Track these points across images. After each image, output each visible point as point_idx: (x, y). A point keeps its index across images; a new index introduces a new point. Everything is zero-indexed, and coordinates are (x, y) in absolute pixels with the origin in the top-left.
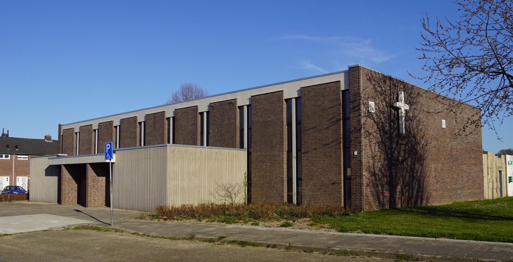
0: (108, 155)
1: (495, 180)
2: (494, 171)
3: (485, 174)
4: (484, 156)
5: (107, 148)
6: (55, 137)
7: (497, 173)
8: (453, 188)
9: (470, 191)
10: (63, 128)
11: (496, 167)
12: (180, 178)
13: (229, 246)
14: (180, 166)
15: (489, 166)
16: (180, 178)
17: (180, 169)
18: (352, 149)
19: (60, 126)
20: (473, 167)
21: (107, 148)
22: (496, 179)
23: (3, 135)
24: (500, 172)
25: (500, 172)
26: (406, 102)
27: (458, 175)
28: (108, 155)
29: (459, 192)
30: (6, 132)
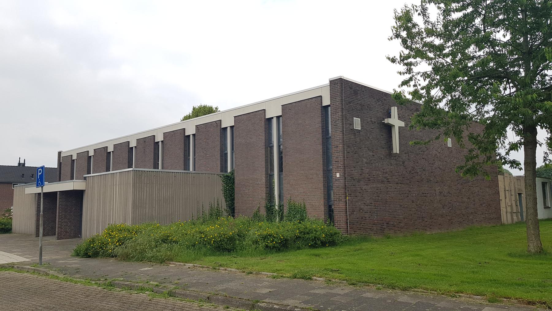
0: (39, 182)
1: (514, 203)
2: (513, 193)
3: (502, 196)
4: (500, 177)
5: (39, 174)
6: (54, 164)
7: (516, 196)
8: (464, 213)
9: (484, 216)
10: (62, 155)
11: (515, 190)
12: (147, 206)
13: (28, 275)
14: (148, 193)
15: (507, 189)
16: (147, 206)
17: (148, 195)
18: (334, 170)
19: (60, 153)
20: (487, 190)
21: (39, 174)
22: (516, 202)
23: (19, 164)
24: (520, 194)
25: (520, 194)
26: (400, 118)
27: (469, 198)
28: (39, 182)
29: (471, 217)
30: (22, 162)
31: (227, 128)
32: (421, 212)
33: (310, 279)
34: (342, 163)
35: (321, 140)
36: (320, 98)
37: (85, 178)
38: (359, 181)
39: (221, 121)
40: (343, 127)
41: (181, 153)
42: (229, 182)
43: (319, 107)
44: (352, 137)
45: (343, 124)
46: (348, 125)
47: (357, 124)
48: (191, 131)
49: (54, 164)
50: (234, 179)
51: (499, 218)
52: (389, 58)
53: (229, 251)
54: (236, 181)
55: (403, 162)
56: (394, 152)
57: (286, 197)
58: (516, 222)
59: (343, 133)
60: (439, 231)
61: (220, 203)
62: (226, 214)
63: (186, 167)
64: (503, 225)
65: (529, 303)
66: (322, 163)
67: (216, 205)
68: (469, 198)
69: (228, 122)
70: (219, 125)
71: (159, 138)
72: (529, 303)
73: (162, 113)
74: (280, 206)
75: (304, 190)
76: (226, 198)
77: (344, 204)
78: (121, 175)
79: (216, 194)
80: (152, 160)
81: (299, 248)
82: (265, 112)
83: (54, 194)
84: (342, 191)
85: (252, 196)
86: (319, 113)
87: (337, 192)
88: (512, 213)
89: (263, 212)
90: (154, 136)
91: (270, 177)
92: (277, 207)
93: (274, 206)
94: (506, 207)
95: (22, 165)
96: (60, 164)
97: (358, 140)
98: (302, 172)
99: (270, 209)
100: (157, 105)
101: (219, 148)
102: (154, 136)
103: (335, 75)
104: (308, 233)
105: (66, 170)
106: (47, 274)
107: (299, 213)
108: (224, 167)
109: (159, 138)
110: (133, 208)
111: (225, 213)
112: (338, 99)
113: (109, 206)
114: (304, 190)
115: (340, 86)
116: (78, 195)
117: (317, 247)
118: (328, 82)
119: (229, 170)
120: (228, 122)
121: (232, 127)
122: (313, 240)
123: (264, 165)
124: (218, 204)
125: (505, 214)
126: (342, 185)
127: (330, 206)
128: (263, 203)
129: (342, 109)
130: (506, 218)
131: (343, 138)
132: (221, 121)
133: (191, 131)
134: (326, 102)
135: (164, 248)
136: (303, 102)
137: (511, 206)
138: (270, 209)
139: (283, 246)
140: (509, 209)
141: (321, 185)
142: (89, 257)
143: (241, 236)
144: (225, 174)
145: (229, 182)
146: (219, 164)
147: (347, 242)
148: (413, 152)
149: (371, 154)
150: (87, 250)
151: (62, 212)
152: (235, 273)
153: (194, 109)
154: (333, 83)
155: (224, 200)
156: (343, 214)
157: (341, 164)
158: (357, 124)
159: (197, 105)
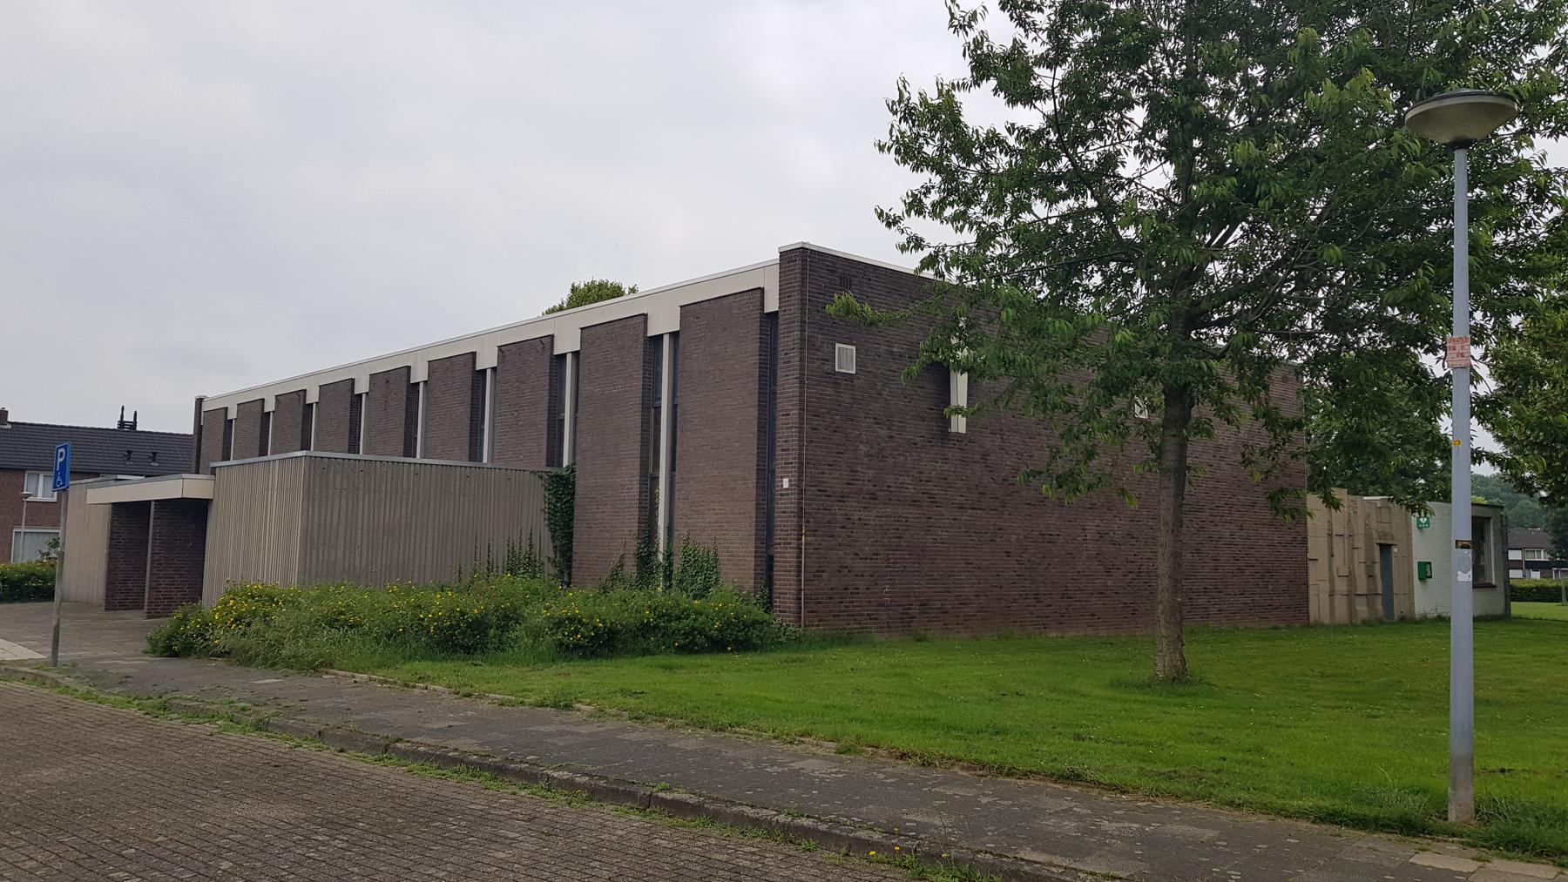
6: (185, 425)
7: (1369, 550)
10: (205, 408)
11: (1368, 536)
12: (341, 543)
16: (341, 543)
19: (200, 401)
23: (122, 423)
27: (1198, 551)
30: (128, 418)
31: (661, 336)
32: (1033, 582)
33: (568, 707)
34: (795, 454)
35: (756, 397)
36: (641, 319)
37: (213, 471)
38: (842, 499)
39: (552, 337)
40: (802, 368)
41: (464, 412)
42: (562, 489)
43: (756, 314)
44: (830, 391)
45: (801, 360)
46: (818, 363)
47: (846, 358)
48: (567, 343)
49: (185, 425)
50: (573, 484)
51: (1302, 606)
52: (880, 215)
53: (469, 650)
54: (578, 490)
55: (985, 456)
56: (953, 429)
57: (681, 532)
58: (1364, 622)
59: (802, 382)
60: (1090, 632)
61: (536, 542)
62: (553, 571)
63: (475, 453)
64: (1308, 625)
65: (1073, 777)
66: (755, 452)
67: (525, 548)
68: (1198, 551)
69: (664, 322)
70: (548, 346)
71: (487, 360)
72: (1073, 777)
73: (495, 293)
74: (669, 555)
75: (714, 519)
76: (553, 531)
77: (794, 553)
78: (284, 469)
79: (530, 520)
80: (401, 430)
81: (646, 652)
82: (646, 322)
83: (144, 506)
84: (793, 522)
85: (608, 531)
86: (754, 329)
87: (785, 522)
88: (1351, 595)
89: (631, 569)
90: (409, 368)
91: (649, 481)
92: (661, 557)
93: (655, 553)
94: (1332, 581)
95: (127, 428)
96: (199, 428)
97: (846, 398)
98: (715, 472)
99: (645, 559)
100: (472, 272)
101: (546, 406)
102: (409, 368)
103: (792, 240)
104: (679, 618)
105: (212, 443)
106: (57, 685)
107: (703, 571)
108: (554, 456)
109: (487, 360)
110: (304, 544)
111: (550, 569)
112: (796, 297)
113: (257, 540)
114: (714, 519)
115: (808, 267)
116: (194, 512)
117: (697, 652)
118: (778, 256)
119: (565, 464)
120: (664, 322)
121: (576, 354)
122: (686, 635)
123: (637, 453)
124: (531, 545)
125: (1325, 597)
126: (793, 507)
127: (771, 558)
128: (633, 546)
129: (803, 322)
130: (1319, 606)
131: (802, 393)
132: (552, 337)
133: (567, 343)
134: (772, 305)
135: (340, 637)
136: (725, 301)
137: (1351, 577)
138: (645, 559)
139: (603, 643)
140: (1342, 586)
141: (751, 507)
142: (176, 655)
143: (509, 618)
144: (554, 470)
145: (562, 489)
146: (544, 446)
147: (797, 642)
148: (1017, 431)
149: (884, 432)
150: (170, 637)
151: (160, 551)
152: (994, 803)
153: (574, 289)
154: (787, 256)
155: (547, 535)
156: (792, 577)
157: (792, 457)
158: (846, 358)
159: (582, 281)
